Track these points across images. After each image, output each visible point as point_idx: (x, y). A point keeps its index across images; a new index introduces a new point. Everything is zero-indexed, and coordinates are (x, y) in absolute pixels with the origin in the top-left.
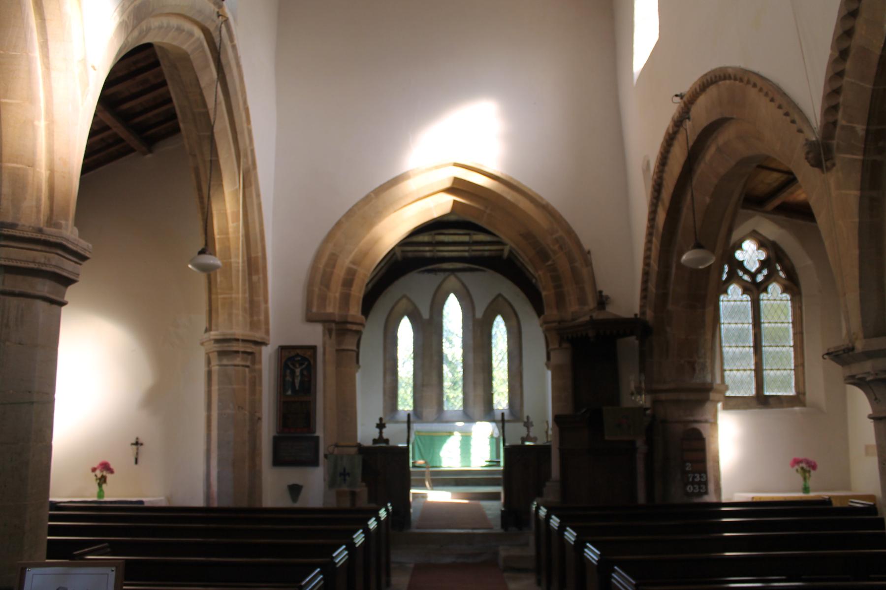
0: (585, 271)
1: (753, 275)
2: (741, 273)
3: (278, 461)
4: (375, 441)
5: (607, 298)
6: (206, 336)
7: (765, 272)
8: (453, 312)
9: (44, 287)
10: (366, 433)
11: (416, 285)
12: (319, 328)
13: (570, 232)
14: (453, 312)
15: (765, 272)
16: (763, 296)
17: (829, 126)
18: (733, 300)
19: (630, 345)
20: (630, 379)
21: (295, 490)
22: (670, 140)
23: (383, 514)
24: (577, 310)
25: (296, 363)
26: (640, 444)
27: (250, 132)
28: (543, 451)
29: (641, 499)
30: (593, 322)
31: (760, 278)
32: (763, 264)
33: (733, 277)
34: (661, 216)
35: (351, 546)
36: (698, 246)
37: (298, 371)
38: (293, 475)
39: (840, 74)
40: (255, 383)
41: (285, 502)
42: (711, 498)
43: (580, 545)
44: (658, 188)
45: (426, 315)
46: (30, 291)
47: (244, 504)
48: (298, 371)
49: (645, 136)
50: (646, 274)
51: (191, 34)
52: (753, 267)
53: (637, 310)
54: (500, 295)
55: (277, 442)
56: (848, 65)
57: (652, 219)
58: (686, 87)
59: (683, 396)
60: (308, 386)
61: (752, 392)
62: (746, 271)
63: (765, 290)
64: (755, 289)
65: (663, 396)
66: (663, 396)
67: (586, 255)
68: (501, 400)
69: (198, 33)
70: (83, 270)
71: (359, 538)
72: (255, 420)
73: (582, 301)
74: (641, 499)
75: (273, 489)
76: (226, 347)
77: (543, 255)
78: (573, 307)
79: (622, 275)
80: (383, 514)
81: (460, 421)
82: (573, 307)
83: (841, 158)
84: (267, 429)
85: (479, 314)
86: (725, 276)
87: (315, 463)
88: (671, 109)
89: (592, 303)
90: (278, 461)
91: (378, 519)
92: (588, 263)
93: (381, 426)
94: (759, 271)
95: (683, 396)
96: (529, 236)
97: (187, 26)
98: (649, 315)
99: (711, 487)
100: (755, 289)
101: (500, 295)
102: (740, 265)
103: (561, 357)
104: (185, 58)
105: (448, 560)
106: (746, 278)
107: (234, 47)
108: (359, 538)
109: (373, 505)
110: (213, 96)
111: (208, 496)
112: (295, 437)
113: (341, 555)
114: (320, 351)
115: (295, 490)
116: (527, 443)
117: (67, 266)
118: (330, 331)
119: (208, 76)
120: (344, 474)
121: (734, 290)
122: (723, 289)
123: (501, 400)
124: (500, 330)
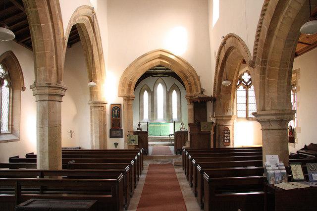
0: (198, 82)
1: (247, 83)
2: (243, 82)
3: (111, 136)
4: (138, 129)
5: (204, 90)
6: (90, 102)
7: (250, 82)
8: (160, 90)
9: (58, 98)
10: (135, 127)
11: (149, 81)
12: (122, 98)
13: (194, 71)
14: (160, 90)
15: (250, 82)
16: (249, 89)
17: (255, 57)
18: (241, 92)
19: (210, 105)
20: (210, 113)
21: (116, 144)
22: (221, 48)
23: (141, 151)
24: (196, 94)
25: (116, 109)
26: (212, 132)
27: (101, 43)
28: (186, 132)
29: (212, 146)
30: (199, 98)
31: (248, 84)
32: (250, 80)
33: (240, 83)
34: (219, 68)
35: (135, 160)
36: (227, 80)
37: (116, 111)
38: (115, 140)
39: (257, 45)
40: (104, 114)
41: (113, 148)
42: (231, 146)
43: (191, 159)
44: (218, 60)
45: (152, 91)
46: (54, 99)
47: (102, 149)
48: (116, 111)
49: (215, 45)
50: (215, 84)
51: (85, 19)
52: (246, 80)
53: (212, 95)
54: (174, 84)
55: (111, 131)
56: (259, 43)
57: (217, 69)
58: (225, 35)
59: (224, 119)
60: (119, 115)
61: (245, 116)
62: (245, 82)
63: (250, 87)
64: (247, 87)
65: (219, 118)
66: (219, 118)
67: (198, 78)
68: (175, 116)
69: (87, 18)
70: (66, 93)
71: (136, 158)
72: (105, 125)
73: (197, 91)
74: (212, 146)
75: (110, 145)
76: (96, 105)
77: (186, 77)
78: (194, 93)
79: (208, 85)
80: (141, 151)
81: (164, 118)
82: (194, 93)
83: (257, 66)
84: (108, 127)
85: (168, 90)
86: (238, 83)
87: (122, 137)
88: (221, 41)
89: (200, 92)
90: (111, 136)
91: (140, 152)
92: (199, 80)
93: (139, 125)
94: (248, 82)
95: (224, 119)
96: (182, 72)
97: (85, 17)
98: (216, 95)
99: (231, 143)
100: (247, 87)
101: (174, 84)
102: (243, 80)
103: (191, 107)
104: (83, 25)
105: (159, 163)
106: (244, 84)
107: (97, 20)
108: (136, 158)
109: (138, 149)
110: (91, 35)
111: (92, 146)
112: (116, 130)
113: (132, 162)
114: (122, 105)
115: (116, 144)
116: (182, 130)
117: (62, 92)
118: (125, 99)
119: (90, 30)
120: (133, 140)
121: (241, 87)
122: (237, 86)
123: (175, 116)
124: (174, 94)
